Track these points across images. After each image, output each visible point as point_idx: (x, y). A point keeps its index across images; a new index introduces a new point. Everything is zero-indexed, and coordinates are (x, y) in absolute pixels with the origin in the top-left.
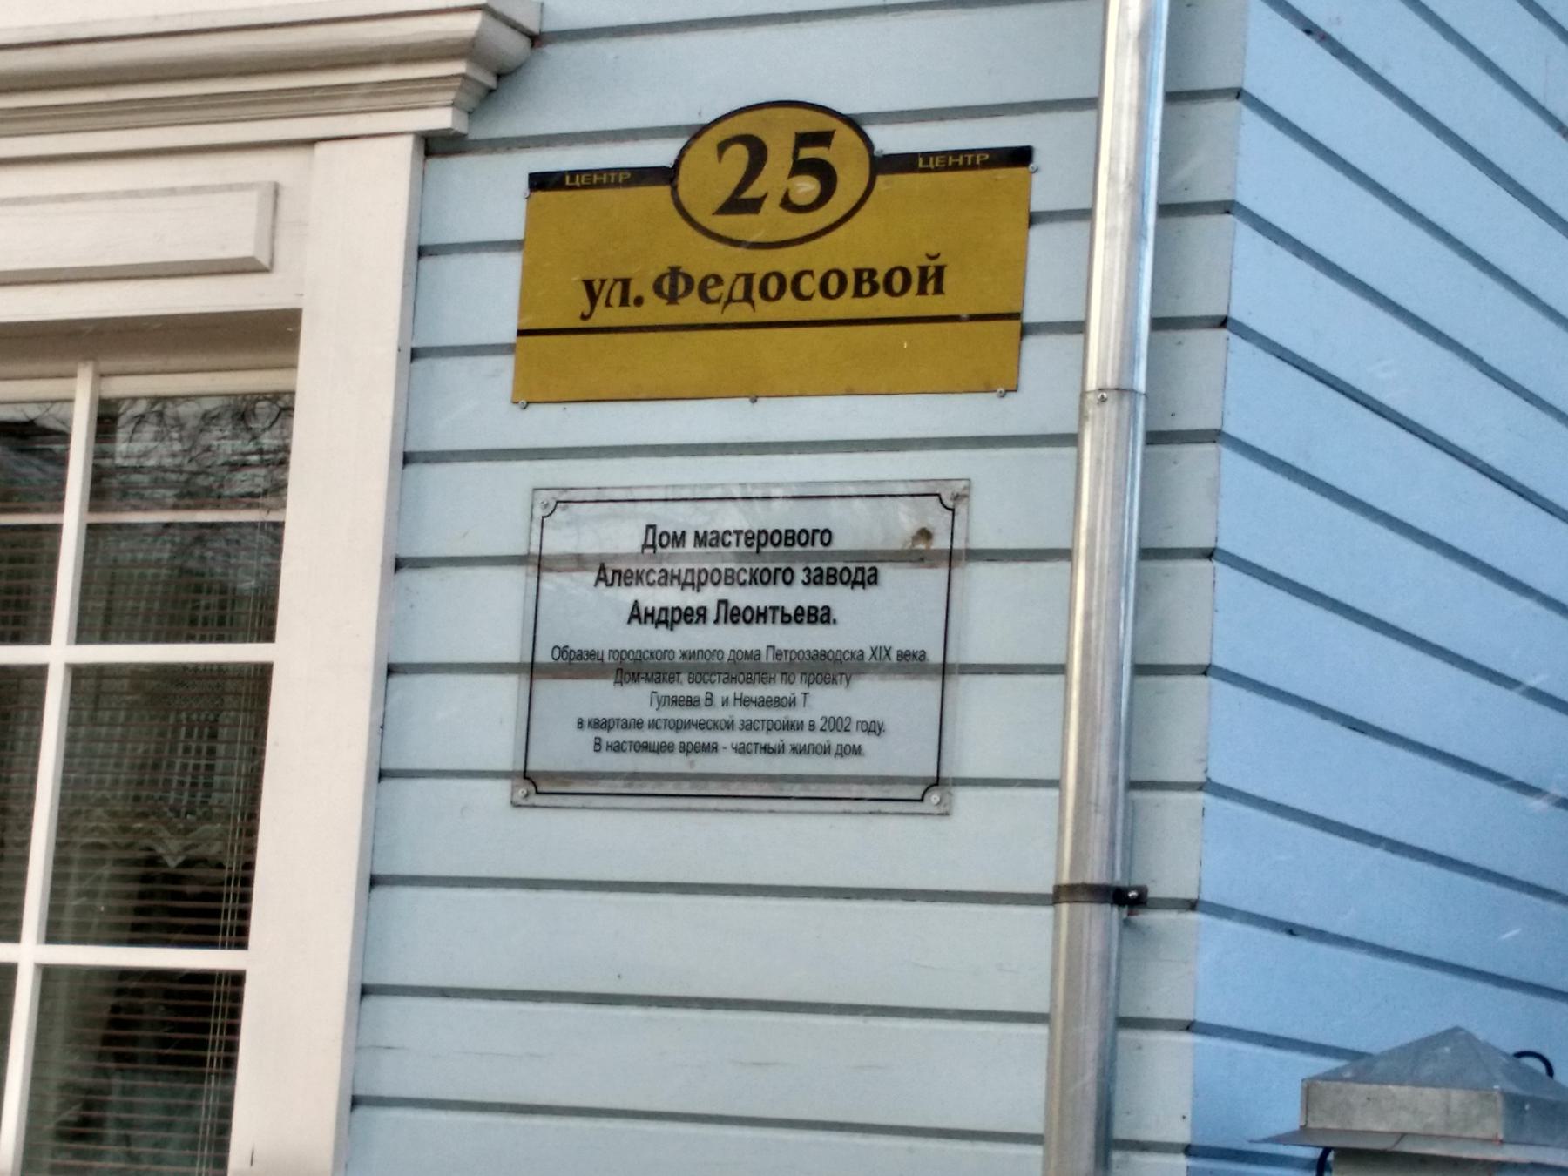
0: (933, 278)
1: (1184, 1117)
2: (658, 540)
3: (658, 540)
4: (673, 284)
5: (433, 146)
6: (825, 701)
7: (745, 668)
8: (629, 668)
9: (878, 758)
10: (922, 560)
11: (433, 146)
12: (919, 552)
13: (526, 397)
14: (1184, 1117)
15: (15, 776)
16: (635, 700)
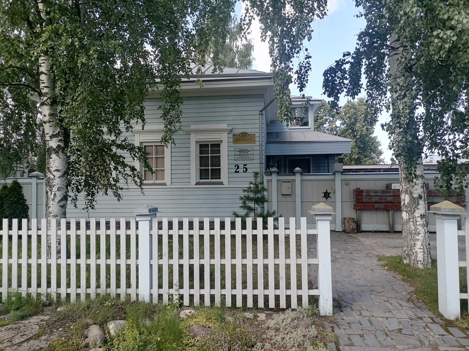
0: (251, 139)
1: (289, 188)
2: (240, 150)
3: (240, 150)
4: (240, 139)
5: (228, 133)
6: (248, 156)
7: (244, 155)
8: (239, 155)
9: (251, 158)
10: (298, 247)
11: (228, 133)
12: (252, 150)
13: (233, 144)
14: (289, 188)
15: (298, 178)
16: (240, 156)
